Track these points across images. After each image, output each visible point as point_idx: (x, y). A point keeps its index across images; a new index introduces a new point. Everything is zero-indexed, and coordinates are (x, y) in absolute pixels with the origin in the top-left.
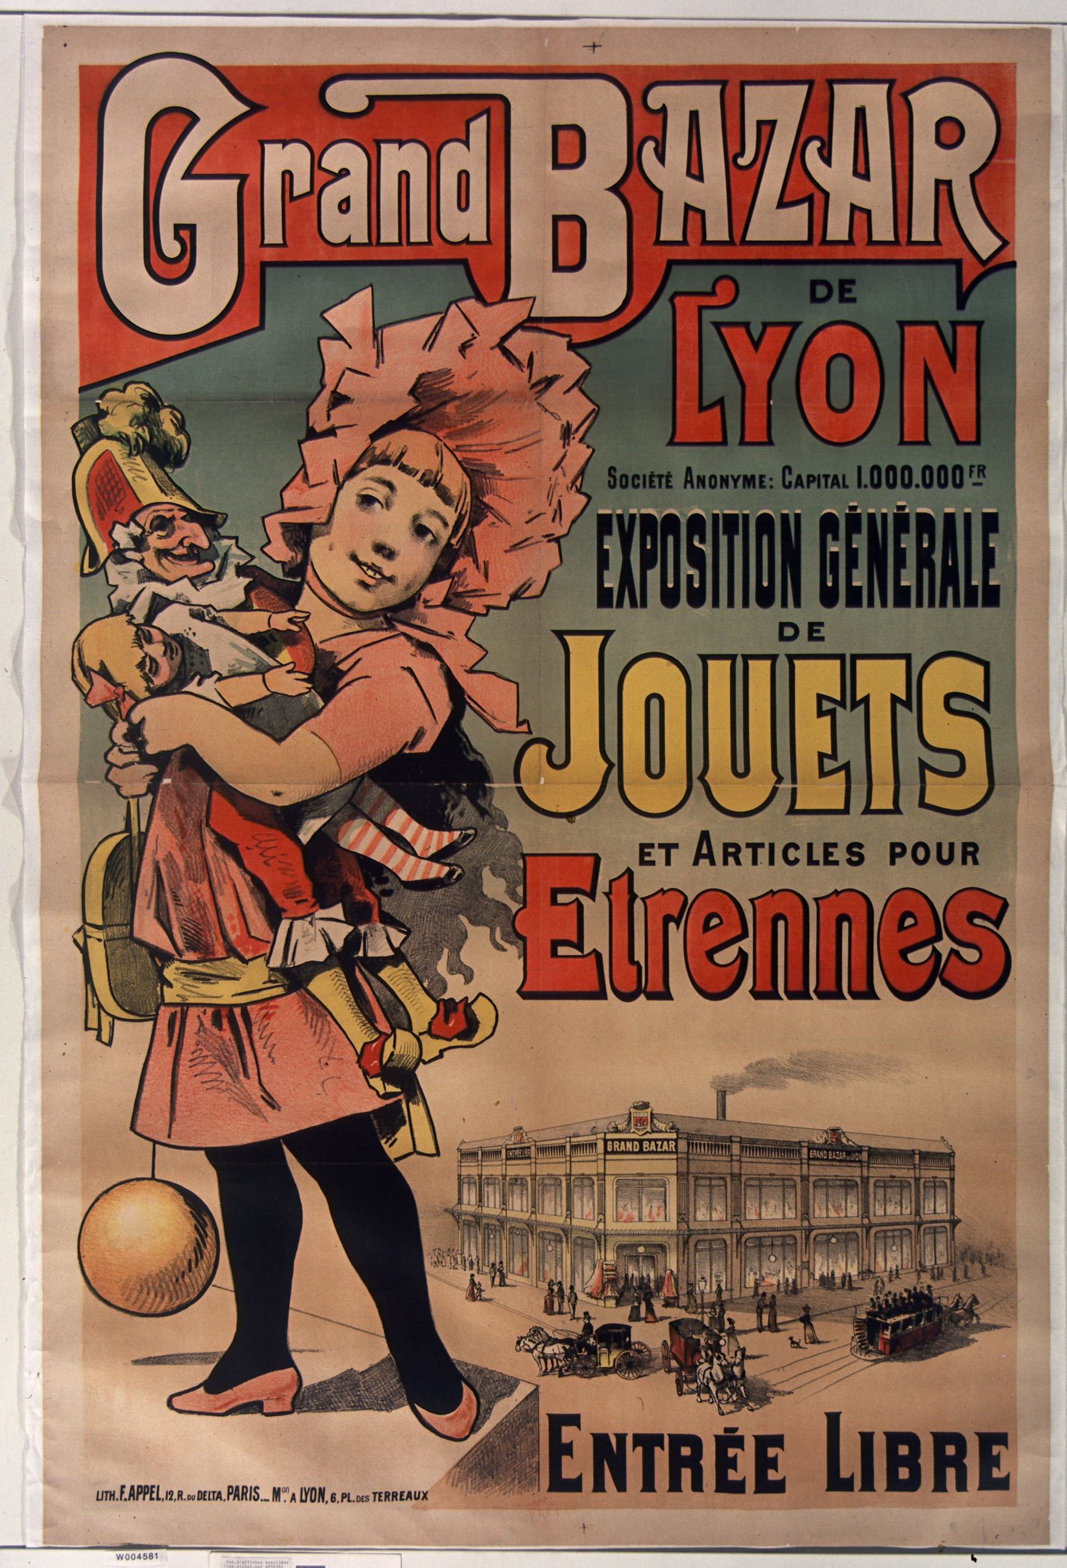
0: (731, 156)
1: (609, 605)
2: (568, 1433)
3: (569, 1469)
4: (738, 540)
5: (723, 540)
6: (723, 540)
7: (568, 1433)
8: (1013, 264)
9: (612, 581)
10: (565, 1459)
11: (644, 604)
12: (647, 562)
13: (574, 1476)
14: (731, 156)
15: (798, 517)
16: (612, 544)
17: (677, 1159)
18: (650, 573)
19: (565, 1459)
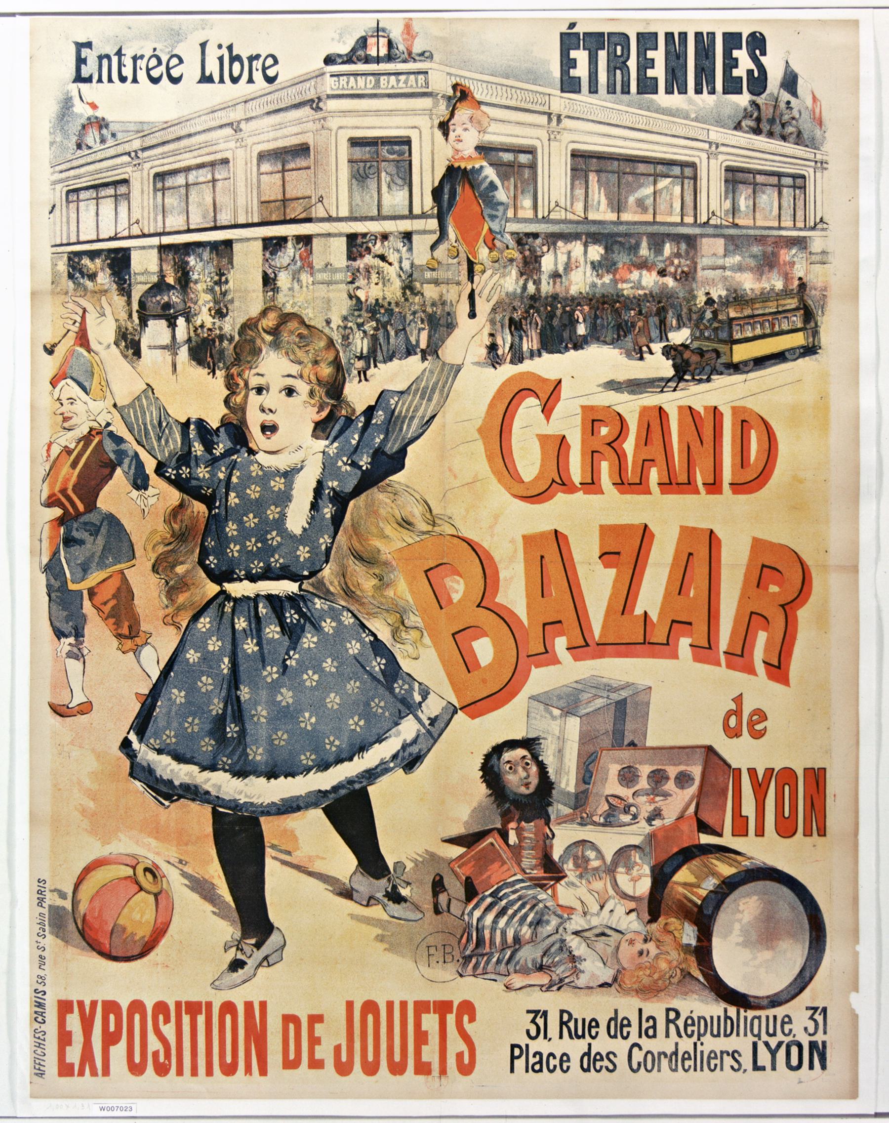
0: (524, 1056)
1: (71, 1074)
2: (85, 52)
3: (85, 72)
4: (201, 1019)
5: (186, 1019)
6: (186, 1019)
7: (85, 52)
8: (641, 358)
9: (74, 1055)
10: (83, 66)
11: (106, 1072)
12: (110, 1039)
13: (87, 76)
14: (524, 1056)
15: (263, 1005)
16: (74, 1022)
17: (116, 196)
18: (113, 1049)
19: (83, 66)
